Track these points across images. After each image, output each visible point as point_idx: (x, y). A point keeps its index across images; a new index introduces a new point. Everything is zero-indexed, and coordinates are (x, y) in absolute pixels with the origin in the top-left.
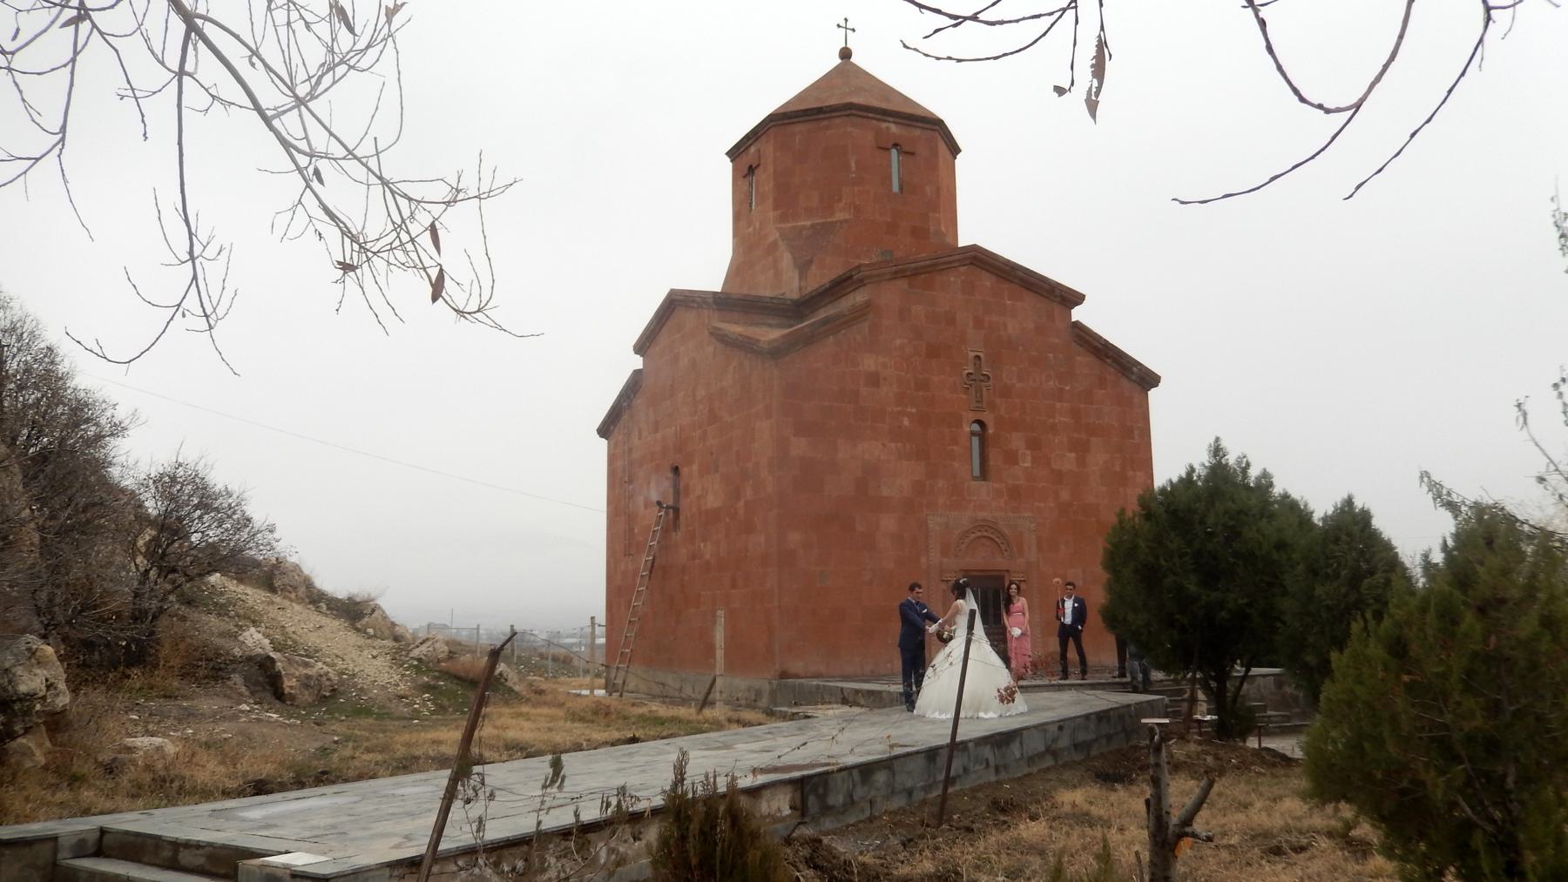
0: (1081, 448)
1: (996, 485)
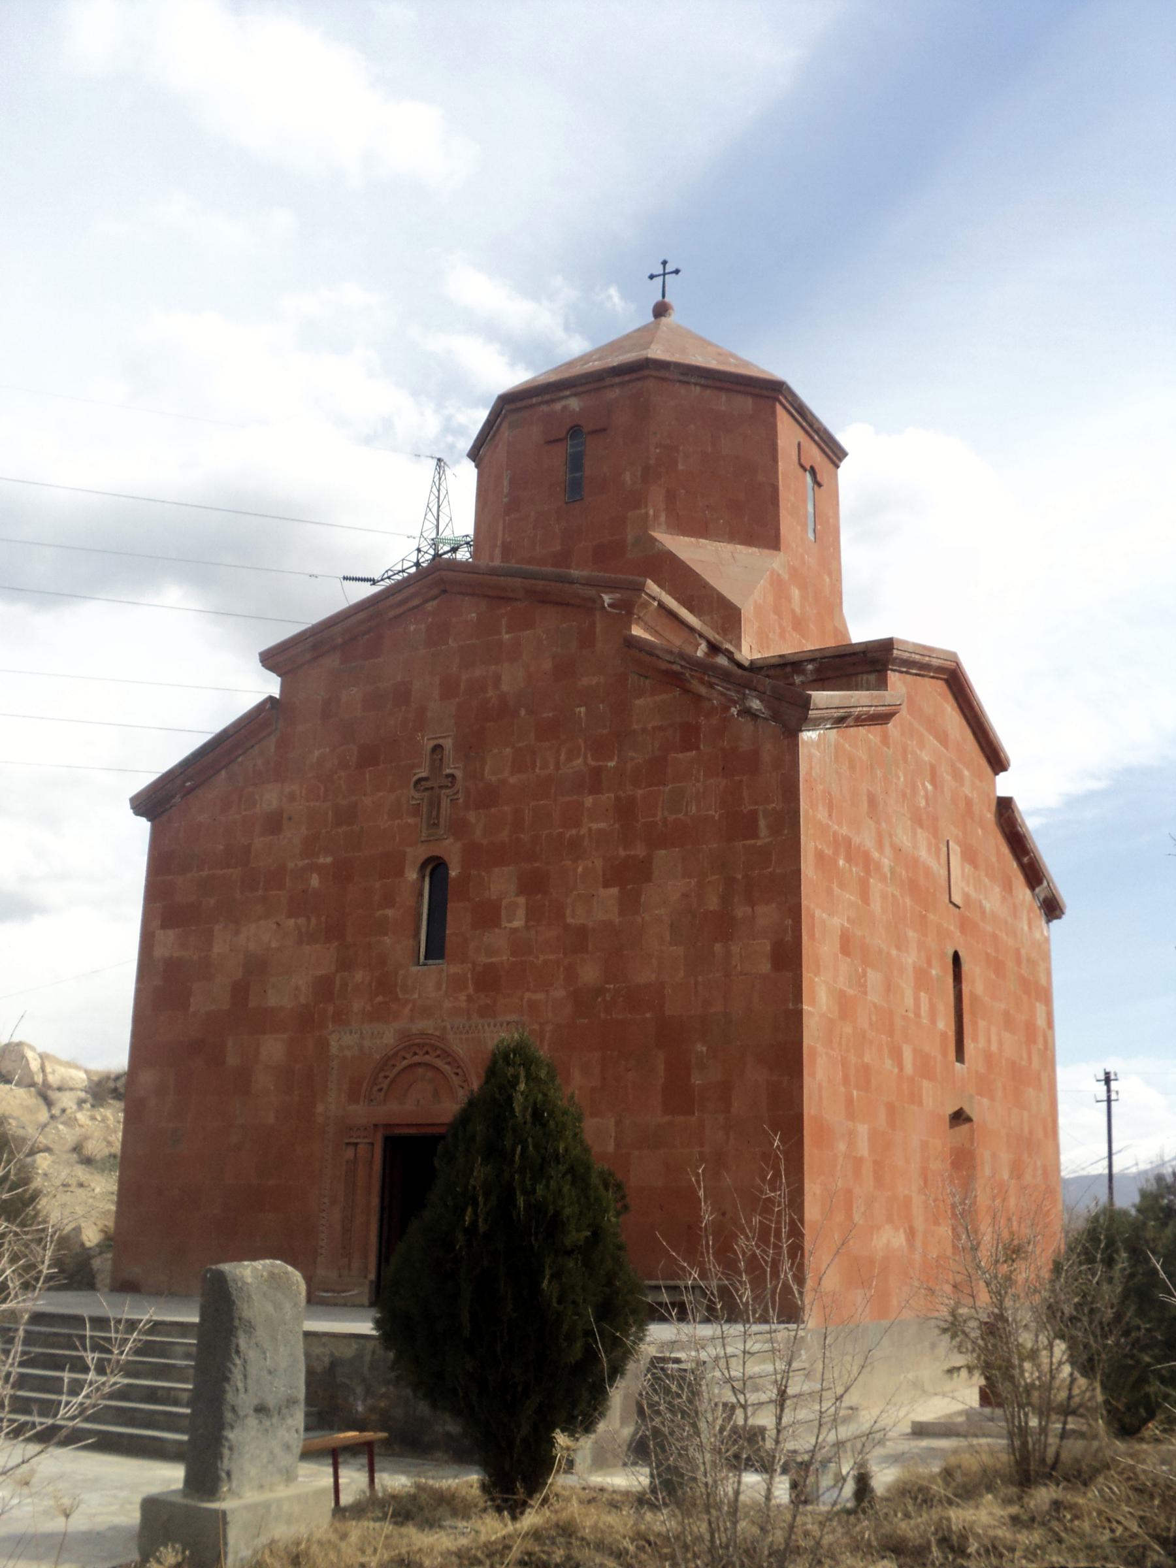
0: (629, 876)
1: (454, 969)
